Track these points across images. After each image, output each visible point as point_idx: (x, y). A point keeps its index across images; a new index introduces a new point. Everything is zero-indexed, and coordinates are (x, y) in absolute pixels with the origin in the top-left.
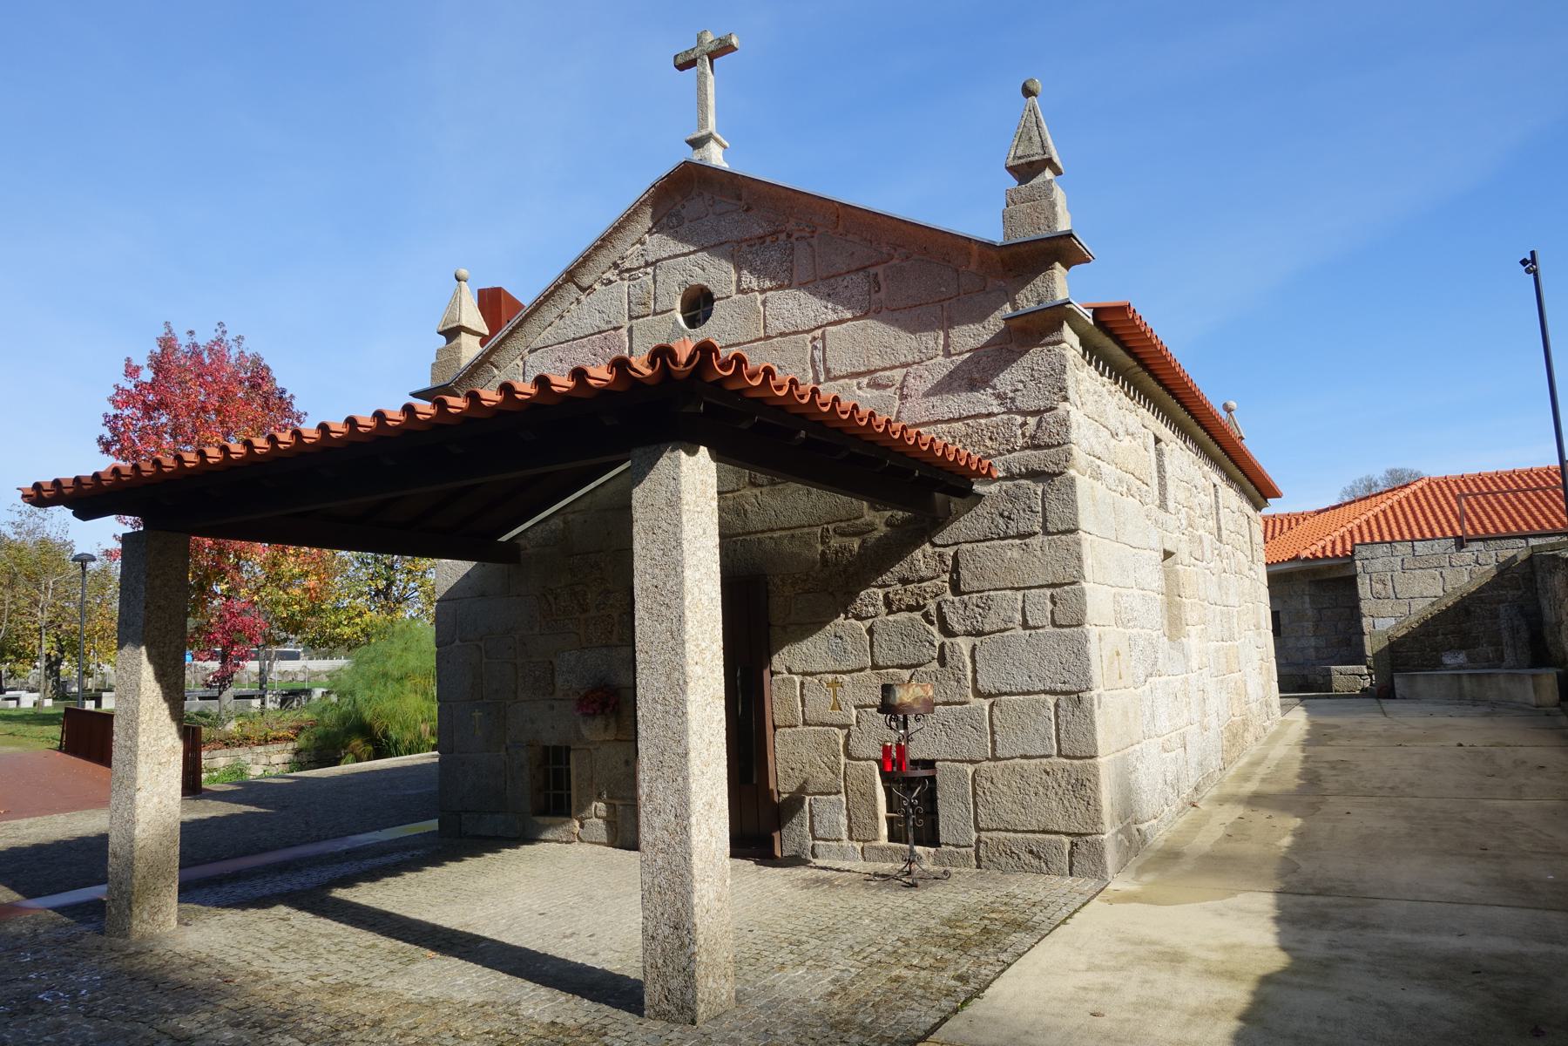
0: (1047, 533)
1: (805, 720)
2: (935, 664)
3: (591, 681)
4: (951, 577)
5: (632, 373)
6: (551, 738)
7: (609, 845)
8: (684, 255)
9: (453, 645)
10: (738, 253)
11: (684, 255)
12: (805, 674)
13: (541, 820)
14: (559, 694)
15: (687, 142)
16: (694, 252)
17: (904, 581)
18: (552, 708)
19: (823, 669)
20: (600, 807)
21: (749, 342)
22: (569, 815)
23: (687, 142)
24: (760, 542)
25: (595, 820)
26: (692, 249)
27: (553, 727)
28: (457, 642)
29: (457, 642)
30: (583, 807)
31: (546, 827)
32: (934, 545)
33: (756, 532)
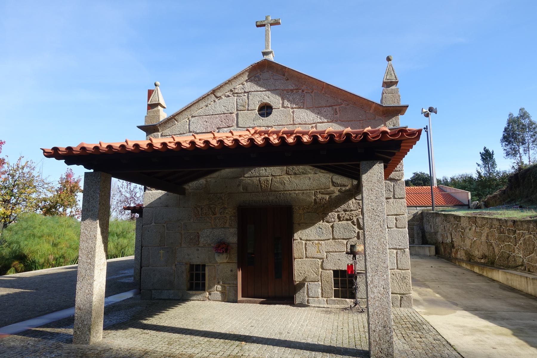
0: (394, 198)
3: (216, 241)
6: (196, 261)
8: (261, 91)
9: (151, 225)
11: (261, 91)
13: (191, 292)
14: (201, 245)
16: (265, 91)
18: (198, 250)
19: (314, 239)
20: (219, 287)
22: (203, 289)
24: (290, 194)
26: (264, 90)
27: (198, 257)
28: (153, 224)
29: (153, 224)
30: (210, 287)
31: (194, 295)
33: (289, 191)
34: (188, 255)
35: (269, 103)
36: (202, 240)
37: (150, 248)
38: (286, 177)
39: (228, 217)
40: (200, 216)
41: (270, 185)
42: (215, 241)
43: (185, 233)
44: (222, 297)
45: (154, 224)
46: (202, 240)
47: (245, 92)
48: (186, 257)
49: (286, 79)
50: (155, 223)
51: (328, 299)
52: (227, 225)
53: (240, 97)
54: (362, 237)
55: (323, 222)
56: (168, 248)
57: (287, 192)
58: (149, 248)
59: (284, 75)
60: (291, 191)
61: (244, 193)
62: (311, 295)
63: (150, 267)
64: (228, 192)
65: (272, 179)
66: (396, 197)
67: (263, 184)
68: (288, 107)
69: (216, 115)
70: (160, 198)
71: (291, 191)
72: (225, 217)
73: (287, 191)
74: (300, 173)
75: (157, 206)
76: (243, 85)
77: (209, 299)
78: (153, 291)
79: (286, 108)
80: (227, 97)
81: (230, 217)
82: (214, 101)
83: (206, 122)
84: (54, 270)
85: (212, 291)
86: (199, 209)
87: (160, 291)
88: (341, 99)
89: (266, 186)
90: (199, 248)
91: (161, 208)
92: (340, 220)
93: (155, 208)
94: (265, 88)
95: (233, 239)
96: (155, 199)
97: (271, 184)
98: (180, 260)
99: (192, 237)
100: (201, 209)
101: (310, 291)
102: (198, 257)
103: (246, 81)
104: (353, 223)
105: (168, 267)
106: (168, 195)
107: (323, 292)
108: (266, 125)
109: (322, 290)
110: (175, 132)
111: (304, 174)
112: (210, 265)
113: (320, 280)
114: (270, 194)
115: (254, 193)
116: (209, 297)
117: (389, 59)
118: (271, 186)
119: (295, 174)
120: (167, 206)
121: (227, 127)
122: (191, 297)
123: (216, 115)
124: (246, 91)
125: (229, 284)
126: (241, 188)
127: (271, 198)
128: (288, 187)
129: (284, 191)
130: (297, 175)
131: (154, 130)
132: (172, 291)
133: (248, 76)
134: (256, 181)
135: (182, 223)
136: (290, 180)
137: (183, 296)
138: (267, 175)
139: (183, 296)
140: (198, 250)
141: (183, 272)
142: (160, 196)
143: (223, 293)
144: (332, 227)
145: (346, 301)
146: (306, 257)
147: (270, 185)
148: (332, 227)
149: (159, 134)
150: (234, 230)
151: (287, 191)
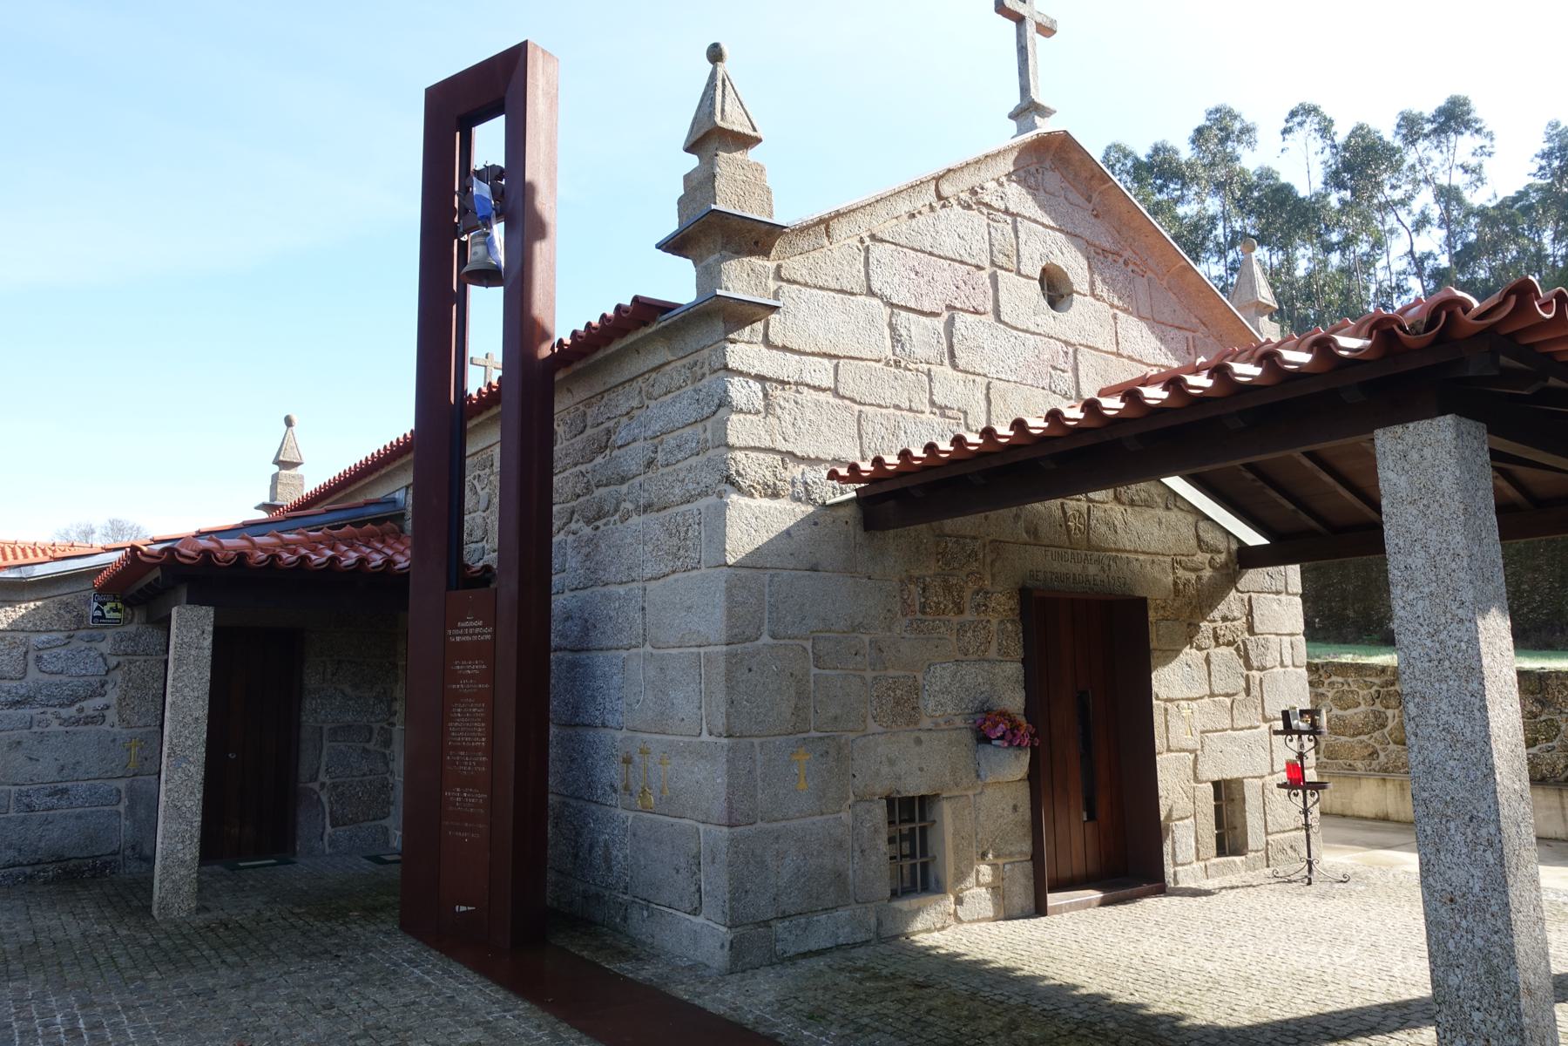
0: (1287, 593)
1: (1169, 746)
2: (1243, 694)
3: (970, 705)
4: (1247, 619)
5: (181, 559)
6: (914, 786)
7: (995, 919)
8: (1043, 225)
9: (759, 643)
10: (1096, 256)
11: (1043, 225)
12: (1166, 700)
13: (904, 904)
14: (926, 723)
15: (659, 246)
16: (1052, 228)
17: (1225, 619)
18: (918, 741)
19: (1180, 697)
20: (985, 872)
21: (1105, 352)
22: (940, 889)
23: (659, 246)
24: (1129, 561)
25: (976, 890)
26: (1052, 224)
27: (921, 769)
28: (766, 639)
29: (766, 639)
30: (961, 877)
31: (916, 913)
32: (1238, 590)
33: (1125, 551)
34: (892, 762)
35: (1065, 270)
36: (929, 704)
37: (756, 741)
38: (1119, 508)
39: (995, 622)
40: (919, 615)
42: (967, 708)
43: (875, 678)
44: (995, 904)
45: (771, 641)
46: (931, 704)
48: (885, 769)
49: (1095, 213)
50: (774, 637)
51: (1208, 863)
52: (993, 652)
53: (996, 221)
54: (1255, 691)
55: (1191, 647)
56: (821, 738)
58: (752, 745)
59: (1089, 200)
62: (1180, 859)
63: (760, 824)
64: (990, 538)
65: (1089, 508)
66: (1290, 590)
68: (1104, 301)
69: (940, 257)
70: (788, 533)
72: (988, 621)
75: (779, 565)
76: (1001, 185)
77: (959, 920)
78: (779, 926)
79: (1098, 300)
80: (964, 208)
81: (1002, 621)
82: (932, 208)
83: (917, 273)
84: (1058, 900)
85: (968, 889)
86: (915, 590)
87: (803, 920)
88: (1196, 316)
90: (924, 736)
91: (793, 573)
92: (1218, 645)
93: (771, 572)
94: (1054, 219)
95: (1014, 701)
96: (772, 536)
98: (866, 785)
99: (899, 693)
100: (924, 590)
101: (1177, 846)
102: (921, 769)
103: (1009, 175)
104: (1237, 649)
105: (825, 817)
106: (816, 524)
107: (1199, 846)
108: (1064, 338)
109: (1197, 841)
110: (824, 277)
111: (1148, 506)
112: (957, 793)
115: (1054, 549)
116: (960, 913)
117: (289, 422)
119: (1132, 503)
120: (814, 569)
121: (973, 313)
122: (907, 925)
123: (940, 257)
124: (1012, 209)
125: (1011, 855)
127: (1093, 569)
128: (1125, 541)
131: (756, 243)
132: (843, 914)
133: (1015, 162)
135: (866, 639)
137: (880, 923)
139: (880, 923)
140: (918, 741)
141: (876, 831)
142: (790, 523)
143: (996, 890)
144: (1208, 661)
145: (1234, 862)
146: (1169, 750)
148: (1208, 661)
149: (771, 265)
150: (1014, 669)
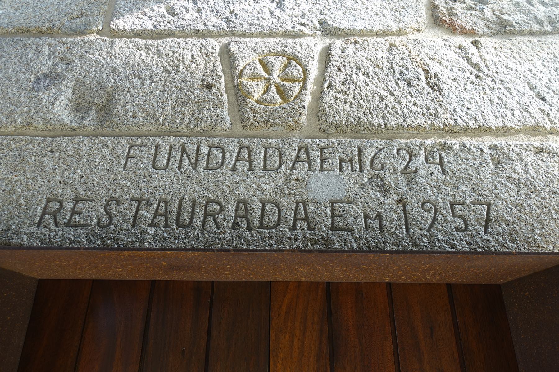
33: (481, 131)
41: (310, 86)
47: (284, 54)
57: (473, 142)
60: (505, 131)
61: (72, 133)
67: (254, 77)
71: (505, 131)
73: (466, 130)
74: (536, 27)
89: (282, 92)
97: (322, 78)
113: (245, 132)
114: (315, 154)
118: (319, 96)
126: (63, 99)
129: (435, 130)
130: (513, 33)
134: (201, 61)
136: (476, 59)
138: (288, 27)
147: (310, 86)
151: (466, 130)
